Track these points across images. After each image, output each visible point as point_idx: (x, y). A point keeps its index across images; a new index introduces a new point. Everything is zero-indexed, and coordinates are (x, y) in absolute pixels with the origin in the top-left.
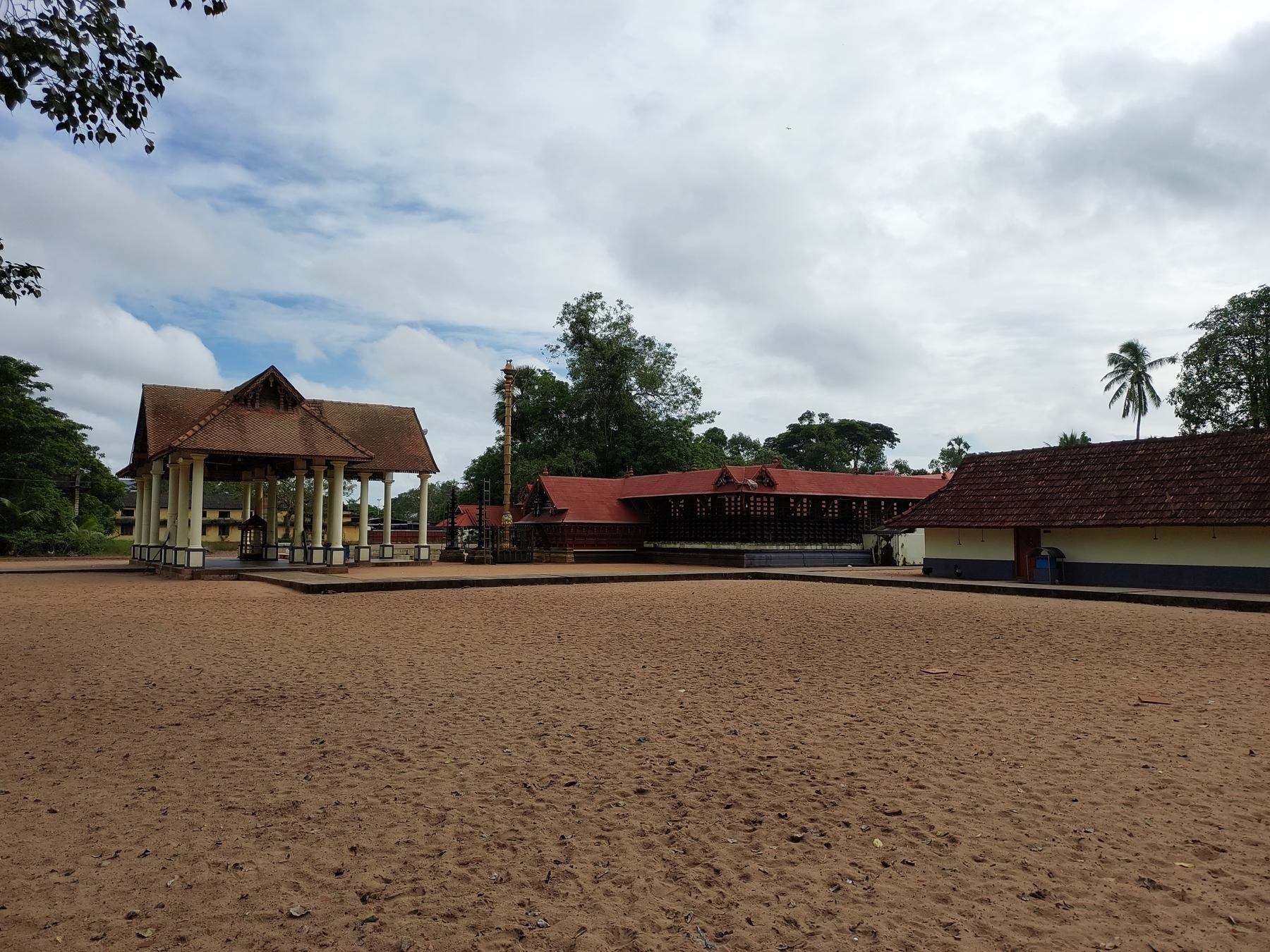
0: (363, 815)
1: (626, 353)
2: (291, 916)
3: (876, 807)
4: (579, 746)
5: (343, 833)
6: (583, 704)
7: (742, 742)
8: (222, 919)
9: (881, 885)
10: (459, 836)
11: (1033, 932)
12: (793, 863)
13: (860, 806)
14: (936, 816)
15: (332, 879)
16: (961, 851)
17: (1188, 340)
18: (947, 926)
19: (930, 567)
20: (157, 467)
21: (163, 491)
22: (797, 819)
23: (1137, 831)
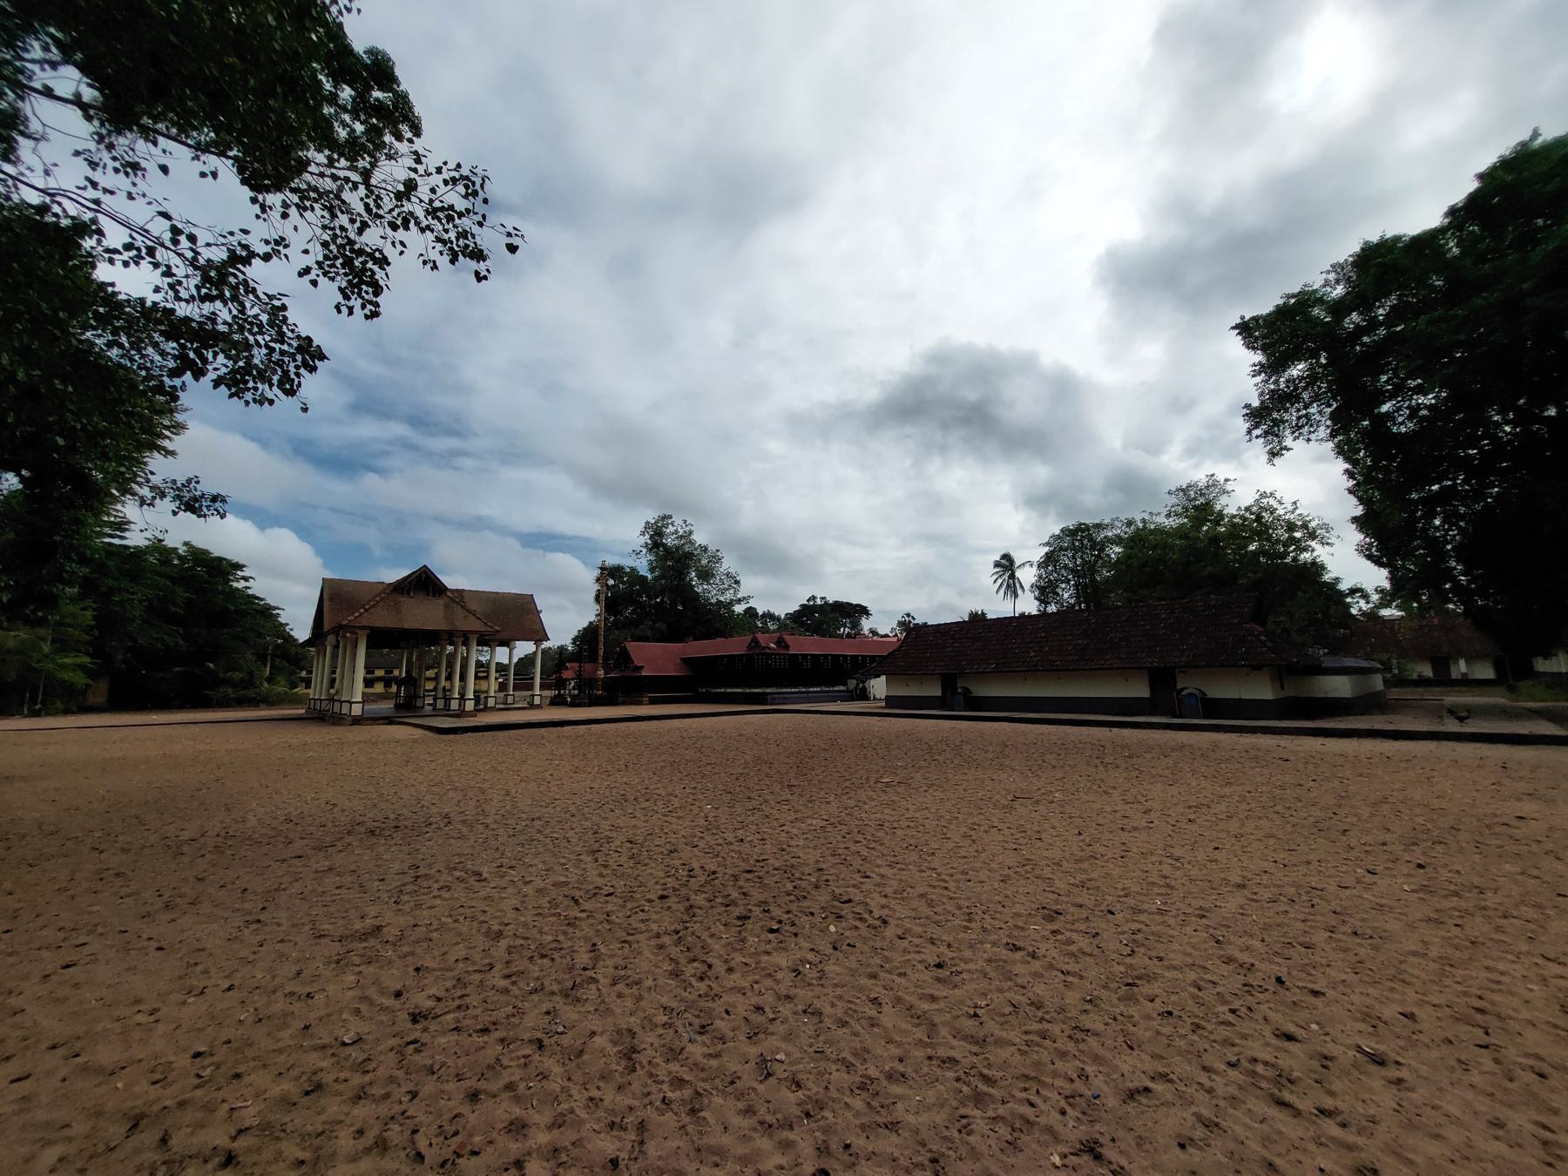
0: (435, 935)
1: (689, 555)
2: (344, 1044)
3: (835, 898)
4: (623, 859)
5: (413, 954)
6: (634, 822)
7: (746, 848)
8: (280, 1051)
9: (830, 968)
10: (509, 950)
11: (933, 999)
12: (768, 953)
13: (822, 897)
14: (875, 901)
15: (389, 1002)
16: (889, 932)
17: (1039, 553)
18: (874, 1001)
19: (891, 701)
20: (331, 639)
21: (335, 656)
22: (777, 912)
23: (1008, 902)
